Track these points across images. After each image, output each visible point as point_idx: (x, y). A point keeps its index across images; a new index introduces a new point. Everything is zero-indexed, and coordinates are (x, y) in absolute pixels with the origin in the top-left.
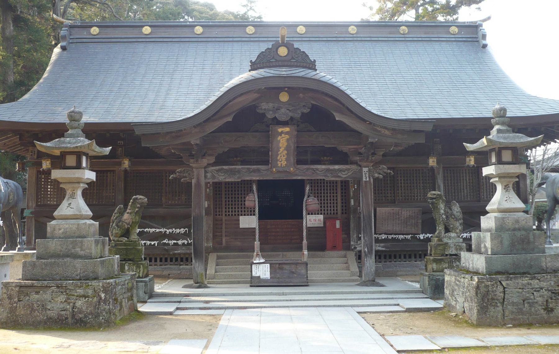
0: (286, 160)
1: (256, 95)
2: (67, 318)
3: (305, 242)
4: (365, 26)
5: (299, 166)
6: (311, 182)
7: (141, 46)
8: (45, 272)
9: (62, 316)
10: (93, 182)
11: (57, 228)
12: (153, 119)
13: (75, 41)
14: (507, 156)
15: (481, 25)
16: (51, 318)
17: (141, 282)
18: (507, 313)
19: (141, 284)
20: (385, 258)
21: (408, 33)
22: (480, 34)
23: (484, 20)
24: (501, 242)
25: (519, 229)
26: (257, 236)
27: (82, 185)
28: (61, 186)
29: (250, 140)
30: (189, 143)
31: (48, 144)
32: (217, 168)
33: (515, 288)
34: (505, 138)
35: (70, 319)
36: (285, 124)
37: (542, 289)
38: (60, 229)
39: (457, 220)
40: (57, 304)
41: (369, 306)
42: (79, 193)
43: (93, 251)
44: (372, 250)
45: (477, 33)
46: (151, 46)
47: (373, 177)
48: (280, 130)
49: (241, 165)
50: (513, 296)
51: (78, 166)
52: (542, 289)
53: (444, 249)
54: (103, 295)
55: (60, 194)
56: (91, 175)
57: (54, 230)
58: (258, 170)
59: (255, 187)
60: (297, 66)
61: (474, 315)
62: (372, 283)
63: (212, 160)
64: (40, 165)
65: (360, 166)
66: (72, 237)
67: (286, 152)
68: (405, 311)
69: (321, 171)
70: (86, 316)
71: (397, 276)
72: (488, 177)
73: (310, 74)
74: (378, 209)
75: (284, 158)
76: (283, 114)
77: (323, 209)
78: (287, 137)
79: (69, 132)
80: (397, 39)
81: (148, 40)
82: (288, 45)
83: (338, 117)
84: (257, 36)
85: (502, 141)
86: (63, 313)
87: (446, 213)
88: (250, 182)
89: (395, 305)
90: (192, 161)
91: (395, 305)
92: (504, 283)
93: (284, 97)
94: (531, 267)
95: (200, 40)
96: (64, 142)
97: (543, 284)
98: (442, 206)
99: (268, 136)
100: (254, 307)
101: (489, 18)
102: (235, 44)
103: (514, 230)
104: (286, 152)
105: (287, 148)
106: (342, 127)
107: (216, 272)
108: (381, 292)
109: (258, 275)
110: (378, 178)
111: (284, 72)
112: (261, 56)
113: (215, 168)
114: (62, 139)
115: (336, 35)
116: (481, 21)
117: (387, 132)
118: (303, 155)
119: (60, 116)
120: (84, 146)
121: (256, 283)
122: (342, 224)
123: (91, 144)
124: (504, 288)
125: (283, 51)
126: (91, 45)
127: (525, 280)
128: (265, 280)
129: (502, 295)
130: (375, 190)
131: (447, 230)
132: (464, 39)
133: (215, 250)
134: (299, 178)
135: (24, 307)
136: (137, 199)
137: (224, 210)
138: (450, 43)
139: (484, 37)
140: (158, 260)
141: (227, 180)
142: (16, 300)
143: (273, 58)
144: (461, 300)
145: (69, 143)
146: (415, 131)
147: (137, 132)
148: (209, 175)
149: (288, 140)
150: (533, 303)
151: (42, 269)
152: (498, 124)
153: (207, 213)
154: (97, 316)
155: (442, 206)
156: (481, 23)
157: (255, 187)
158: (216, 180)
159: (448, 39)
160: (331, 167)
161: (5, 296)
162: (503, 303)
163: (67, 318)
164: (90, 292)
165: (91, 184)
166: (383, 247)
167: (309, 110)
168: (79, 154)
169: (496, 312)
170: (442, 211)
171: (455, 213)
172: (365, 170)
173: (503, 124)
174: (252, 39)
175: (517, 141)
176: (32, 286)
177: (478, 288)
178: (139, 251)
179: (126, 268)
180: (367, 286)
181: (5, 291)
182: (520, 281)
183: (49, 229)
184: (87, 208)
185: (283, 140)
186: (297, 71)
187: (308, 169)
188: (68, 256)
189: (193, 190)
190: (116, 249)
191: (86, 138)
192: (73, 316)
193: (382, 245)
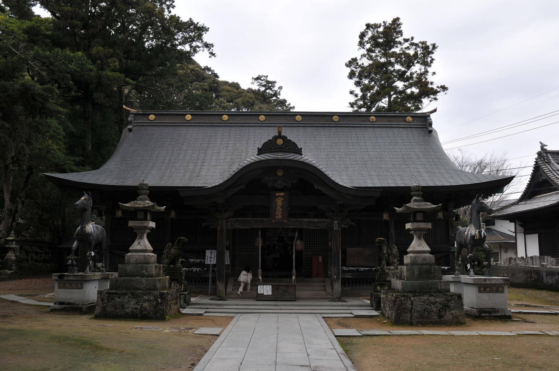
0: (282, 214)
4: (342, 116)
7: (184, 129)
11: (131, 257)
12: (192, 185)
13: (138, 124)
14: (420, 217)
15: (429, 116)
16: (127, 314)
17: (183, 294)
19: (183, 296)
20: (352, 283)
21: (376, 121)
22: (428, 122)
24: (413, 272)
25: (426, 264)
27: (147, 231)
31: (127, 205)
32: (235, 219)
36: (280, 190)
37: (436, 302)
39: (395, 257)
40: (131, 305)
41: (332, 313)
42: (145, 236)
43: (154, 273)
44: (339, 277)
46: (191, 129)
48: (277, 194)
51: (145, 219)
53: (386, 278)
54: (160, 300)
55: (133, 236)
57: (130, 259)
59: (260, 233)
60: (289, 152)
62: (339, 299)
65: (332, 219)
66: (141, 264)
67: (281, 209)
68: (355, 317)
69: (305, 222)
70: (149, 313)
71: (360, 296)
72: (409, 230)
73: (297, 157)
74: (349, 250)
75: (280, 213)
78: (282, 199)
81: (189, 124)
82: (284, 138)
84: (267, 122)
85: (416, 207)
86: (134, 310)
88: (258, 229)
89: (349, 313)
91: (349, 313)
92: (412, 299)
93: (280, 173)
96: (137, 204)
97: (438, 300)
100: (256, 313)
101: (435, 111)
102: (251, 128)
103: (422, 265)
104: (281, 209)
105: (282, 207)
107: (233, 290)
108: (343, 306)
109: (262, 293)
110: (344, 228)
113: (233, 219)
114: (136, 201)
115: (323, 123)
116: (429, 112)
118: (293, 212)
119: (131, 181)
120: (149, 207)
121: (262, 298)
124: (412, 302)
125: (280, 142)
126: (149, 128)
127: (425, 297)
128: (267, 296)
129: (410, 306)
130: (342, 236)
131: (388, 264)
136: (180, 239)
138: (406, 129)
139: (431, 124)
140: (193, 281)
141: (241, 228)
143: (273, 146)
144: (387, 309)
146: (368, 197)
148: (229, 224)
149: (282, 201)
150: (430, 311)
157: (260, 233)
158: (234, 228)
160: (313, 220)
162: (411, 311)
163: (137, 314)
164: (152, 298)
165: (152, 229)
166: (351, 276)
168: (145, 210)
171: (394, 252)
172: (336, 222)
173: (418, 196)
174: (263, 125)
175: (426, 207)
176: (116, 293)
178: (181, 274)
179: (173, 285)
183: (126, 258)
184: (150, 246)
185: (280, 200)
190: (167, 272)
191: (150, 200)
192: (141, 313)
193: (350, 274)
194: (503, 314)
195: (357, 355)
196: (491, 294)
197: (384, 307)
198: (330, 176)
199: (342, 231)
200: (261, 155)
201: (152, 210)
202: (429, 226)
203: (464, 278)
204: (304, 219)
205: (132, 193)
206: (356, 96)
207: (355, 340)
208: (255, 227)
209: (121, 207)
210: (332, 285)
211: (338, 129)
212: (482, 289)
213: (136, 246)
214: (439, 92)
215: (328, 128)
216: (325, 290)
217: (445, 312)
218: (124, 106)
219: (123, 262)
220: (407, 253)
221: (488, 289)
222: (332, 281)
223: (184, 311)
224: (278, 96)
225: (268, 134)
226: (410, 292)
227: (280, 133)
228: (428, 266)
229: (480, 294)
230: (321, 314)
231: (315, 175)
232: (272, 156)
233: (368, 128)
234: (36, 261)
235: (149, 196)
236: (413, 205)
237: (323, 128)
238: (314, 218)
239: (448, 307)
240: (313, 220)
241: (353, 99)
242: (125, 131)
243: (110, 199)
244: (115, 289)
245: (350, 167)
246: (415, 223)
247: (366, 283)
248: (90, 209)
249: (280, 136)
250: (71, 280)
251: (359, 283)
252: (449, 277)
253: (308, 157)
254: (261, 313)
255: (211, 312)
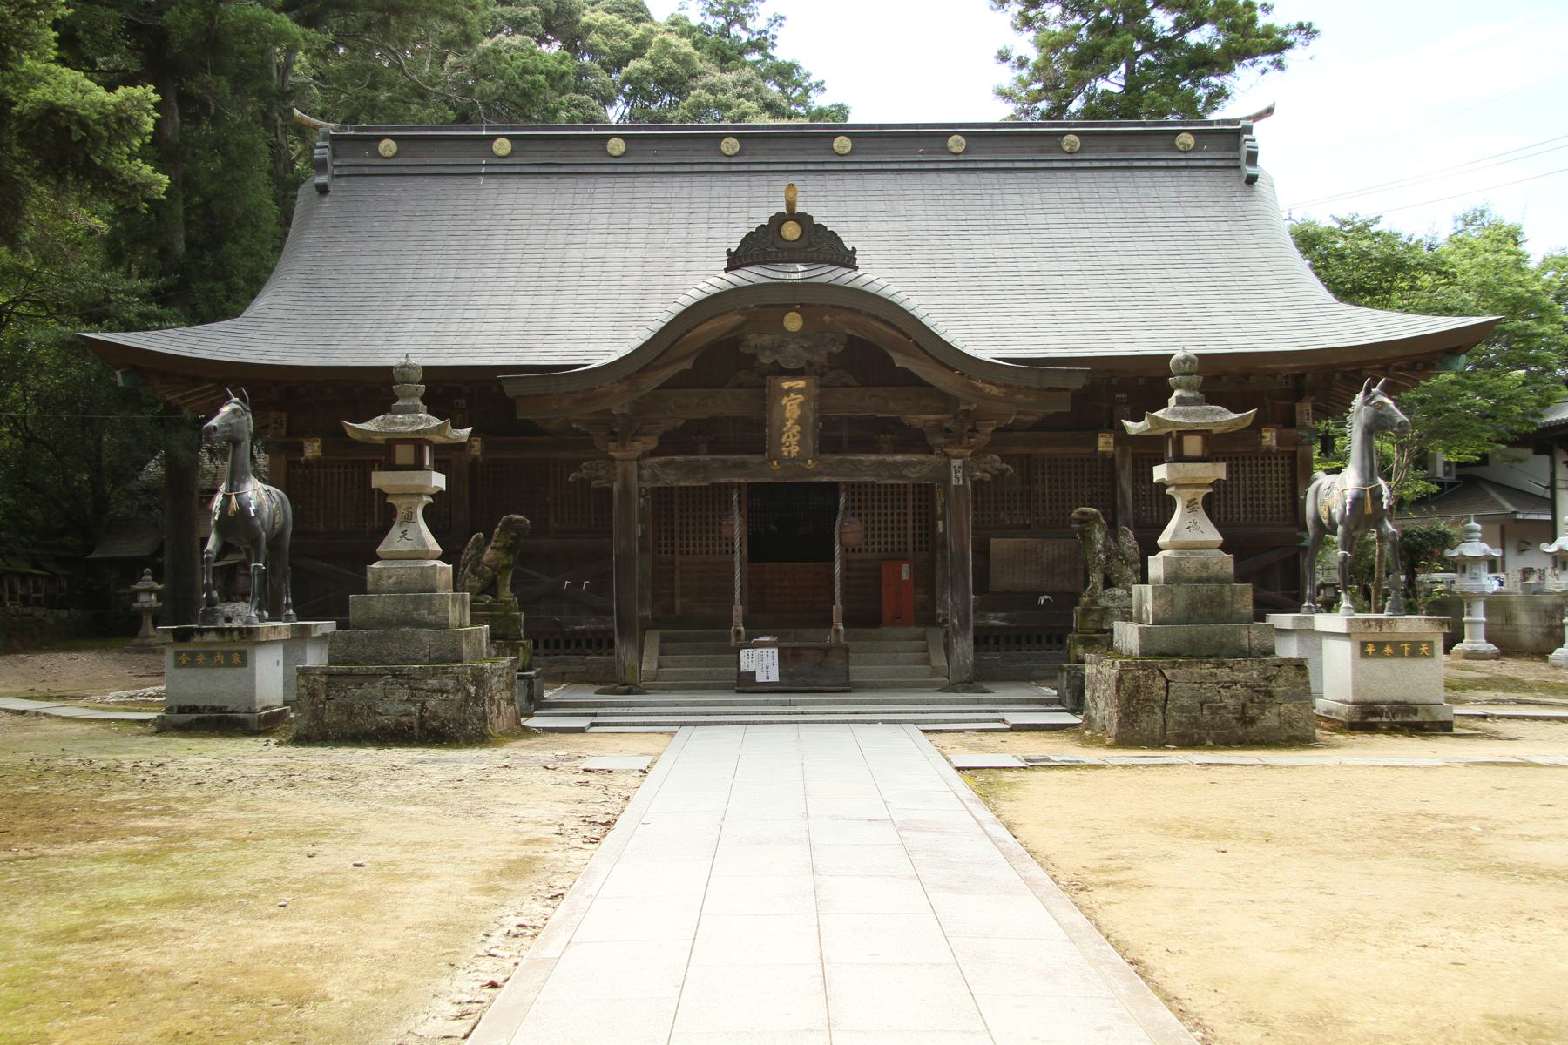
0: (799, 443)
1: (734, 319)
2: (411, 728)
3: (837, 608)
4: (982, 137)
5: (823, 456)
6: (851, 486)
8: (369, 651)
9: (402, 724)
10: (441, 492)
11: (385, 574)
15: (1249, 130)
18: (1170, 724)
20: (1008, 641)
21: (1081, 151)
22: (1244, 150)
23: (1258, 117)
24: (1172, 601)
25: (1209, 580)
26: (737, 595)
28: (389, 500)
29: (726, 404)
30: (608, 412)
33: (1186, 683)
34: (1186, 415)
35: (416, 731)
38: (390, 577)
39: (1128, 563)
40: (395, 706)
41: (946, 721)
42: (420, 512)
44: (967, 622)
45: (1237, 148)
47: (972, 477)
48: (786, 385)
49: (710, 452)
50: (1183, 695)
51: (418, 466)
52: (1235, 683)
53: (1101, 620)
54: (472, 689)
55: (385, 515)
56: (439, 481)
57: (380, 577)
58: (744, 465)
61: (1113, 728)
63: (651, 443)
64: (300, 450)
66: (413, 591)
67: (798, 428)
69: (867, 466)
72: (1162, 486)
74: (998, 545)
75: (794, 441)
76: (792, 355)
77: (870, 540)
78: (801, 398)
79: (400, 403)
80: (1055, 165)
82: (804, 220)
83: (899, 361)
87: (1107, 549)
88: (721, 493)
89: (997, 721)
90: (612, 445)
92: (1167, 673)
93: (793, 322)
94: (1222, 645)
95: (619, 169)
96: (394, 423)
97: (1240, 676)
98: (1099, 536)
99: (764, 399)
103: (1199, 580)
104: (798, 428)
105: (799, 421)
106: (910, 380)
108: (979, 702)
110: (982, 481)
111: (799, 272)
112: (749, 240)
115: (919, 158)
116: (1248, 118)
117: (995, 391)
118: (830, 435)
121: (747, 684)
122: (914, 572)
123: (444, 426)
124: (1167, 682)
125: (791, 231)
126: (382, 182)
127: (1206, 669)
129: (1163, 693)
130: (975, 502)
131: (1108, 583)
132: (1207, 163)
133: (656, 623)
134: (825, 479)
135: (337, 709)
137: (677, 542)
139: (1252, 158)
141: (682, 484)
142: (323, 697)
144: (1101, 704)
145: (403, 424)
147: (510, 392)
148: (646, 473)
149: (801, 405)
151: (364, 646)
152: (1179, 387)
153: (643, 549)
154: (464, 725)
155: (1099, 536)
156: (1249, 123)
159: (1171, 164)
160: (889, 458)
161: (304, 690)
163: (411, 728)
164: (451, 684)
165: (438, 495)
166: (1003, 619)
167: (842, 348)
168: (417, 442)
169: (1151, 722)
170: (1099, 546)
172: (956, 463)
173: (1188, 387)
174: (734, 168)
176: (349, 674)
177: (1120, 680)
180: (956, 691)
181: (303, 682)
182: (1196, 670)
183: (369, 576)
185: (792, 401)
186: (819, 272)
187: (841, 462)
188: (406, 623)
189: (616, 502)
192: (422, 724)
194: (1428, 719)
195: (1005, 806)
196: (1396, 662)
197: (1093, 699)
198: (938, 329)
199: (975, 488)
200: (738, 272)
201: (438, 439)
202: (1219, 471)
203: (1323, 622)
204: (862, 457)
205: (372, 388)
206: (1022, 63)
207: (1008, 777)
208: (722, 480)
209: (350, 433)
210: (948, 649)
211: (963, 176)
212: (1370, 649)
213: (394, 542)
214: (1290, 46)
215: (933, 175)
216: (927, 661)
217: (1262, 716)
218: (297, 112)
219: (362, 589)
220: (1156, 549)
221: (1388, 649)
222: (946, 635)
223: (530, 723)
224: (770, 51)
225: (751, 205)
226: (1162, 655)
227: (791, 205)
228: (1213, 586)
229: (1365, 663)
230: (916, 722)
231: (895, 327)
232: (769, 273)
233: (1058, 174)
234: (25, 601)
235: (423, 400)
236: (1170, 413)
237: (918, 176)
238: (896, 452)
239: (1269, 694)
240: (889, 458)
241: (1007, 76)
242: (305, 193)
243: (314, 409)
244: (345, 663)
245: (1008, 287)
246: (1179, 465)
247: (1049, 641)
248: (248, 440)
249: (792, 215)
250: (210, 643)
251: (1029, 642)
252: (1283, 620)
253: (881, 270)
254: (747, 723)
255: (608, 725)
